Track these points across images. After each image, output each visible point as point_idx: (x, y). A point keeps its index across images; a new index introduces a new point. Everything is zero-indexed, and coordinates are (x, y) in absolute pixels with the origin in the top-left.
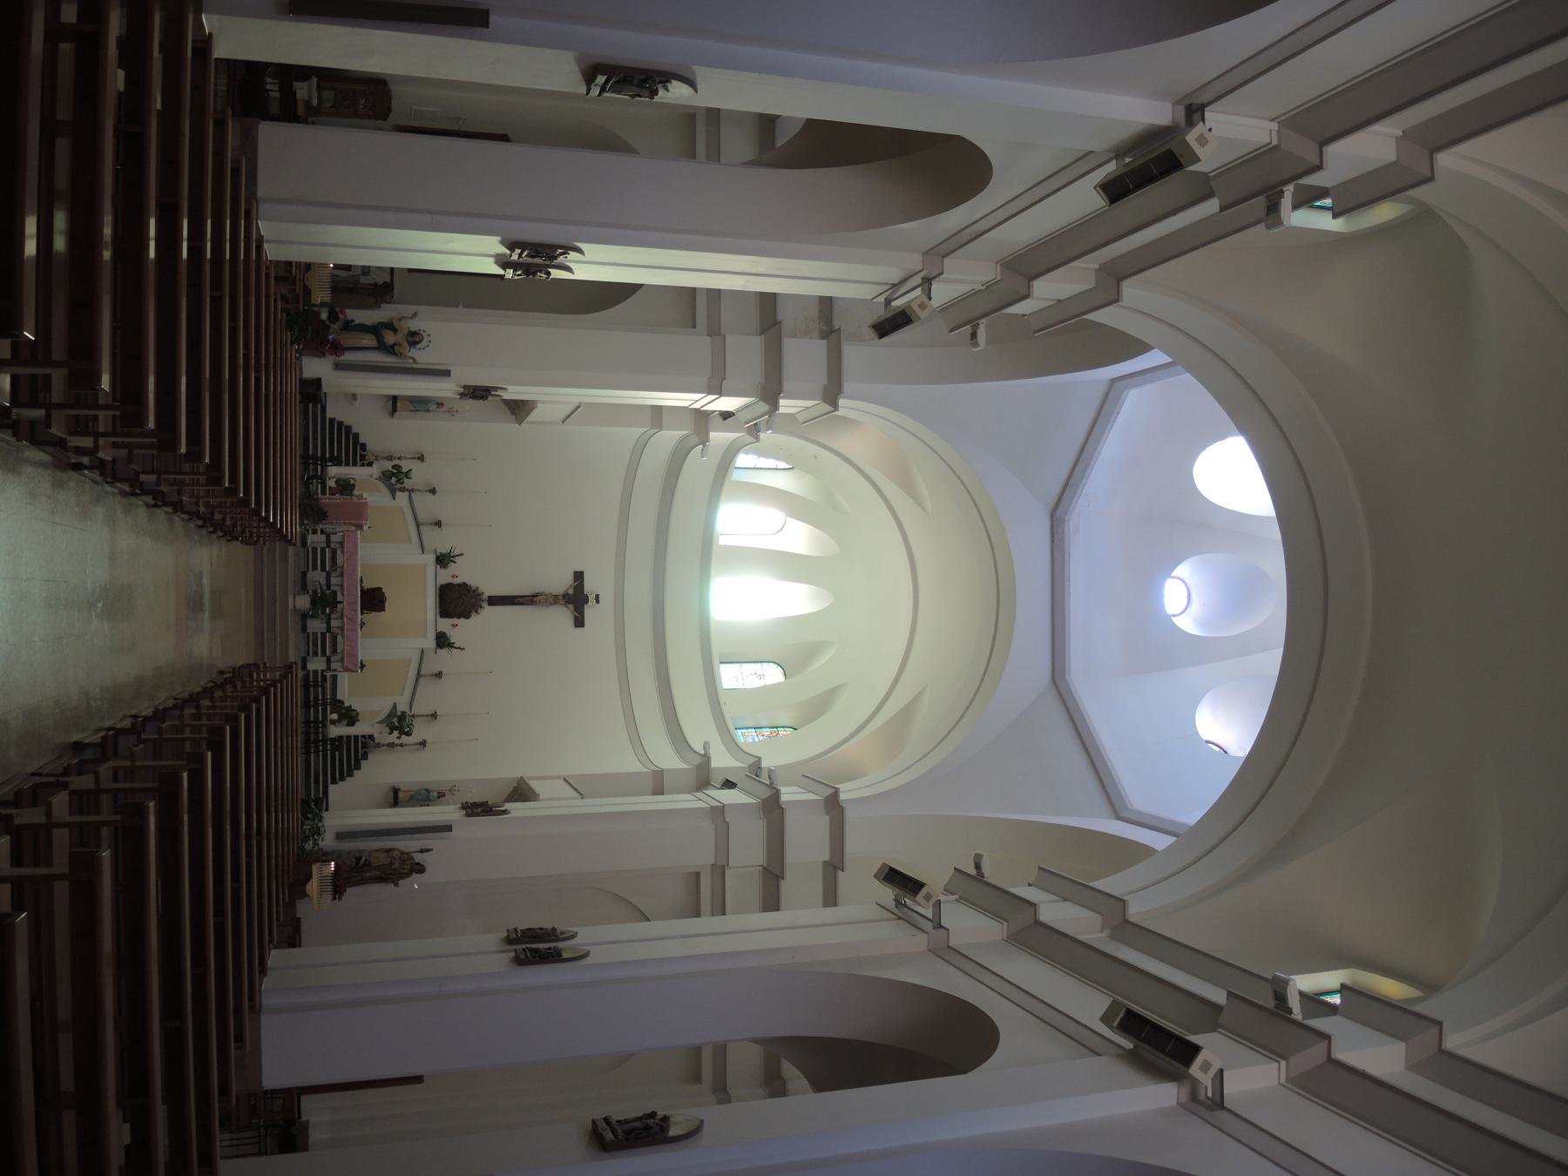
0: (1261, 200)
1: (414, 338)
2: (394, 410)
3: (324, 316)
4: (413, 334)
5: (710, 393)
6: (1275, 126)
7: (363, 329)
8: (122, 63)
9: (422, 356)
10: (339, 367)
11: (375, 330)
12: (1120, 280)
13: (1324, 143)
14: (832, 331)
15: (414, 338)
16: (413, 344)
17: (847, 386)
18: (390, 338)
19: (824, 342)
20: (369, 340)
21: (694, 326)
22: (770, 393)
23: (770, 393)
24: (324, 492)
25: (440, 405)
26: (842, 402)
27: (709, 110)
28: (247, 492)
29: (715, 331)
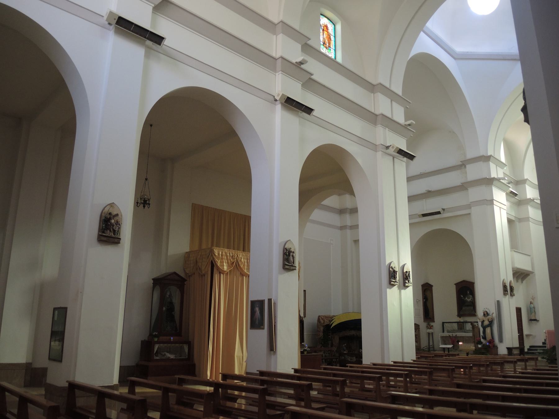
0: (302, 66)
1: (486, 314)
2: (535, 320)
3: (480, 346)
4: (484, 315)
5: (493, 204)
6: (277, 74)
7: (484, 332)
8: (432, 408)
9: (493, 310)
10: (501, 340)
11: (484, 328)
12: (374, 85)
13: (275, 59)
14: (463, 164)
15: (486, 314)
16: (488, 314)
17: (482, 153)
18: (486, 323)
19: (467, 166)
20: (488, 330)
21: (470, 214)
22: (489, 182)
23: (489, 182)
24: (545, 347)
25: (531, 303)
26: (489, 154)
27: (409, 219)
28: (342, 376)
29: (469, 206)
